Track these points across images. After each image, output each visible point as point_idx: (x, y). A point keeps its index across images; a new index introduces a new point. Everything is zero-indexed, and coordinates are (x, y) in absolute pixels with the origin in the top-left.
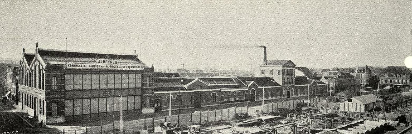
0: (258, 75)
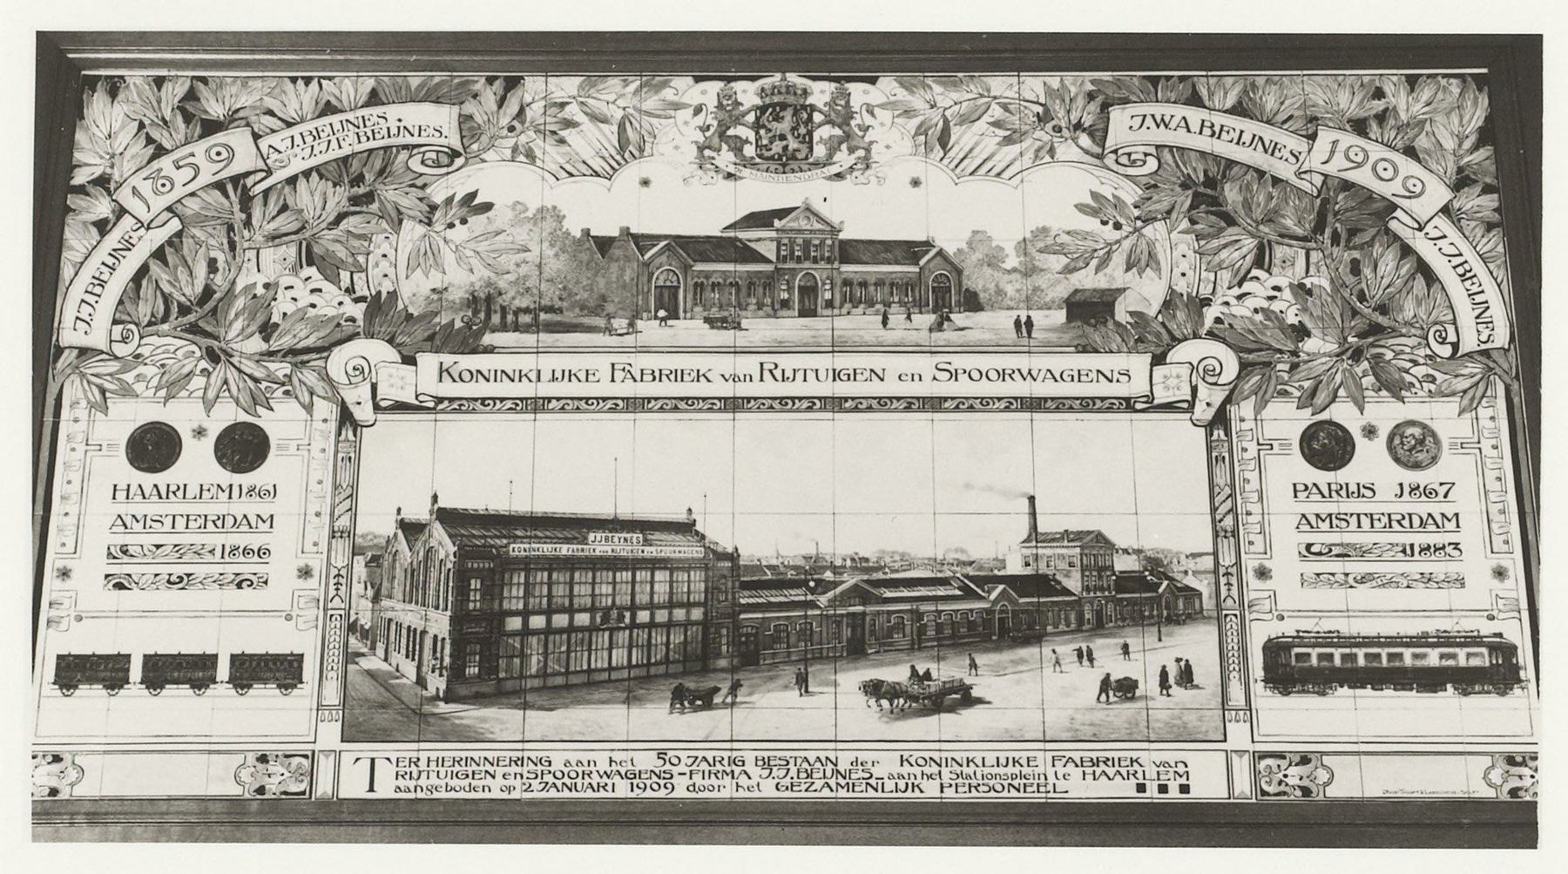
0: (1015, 567)
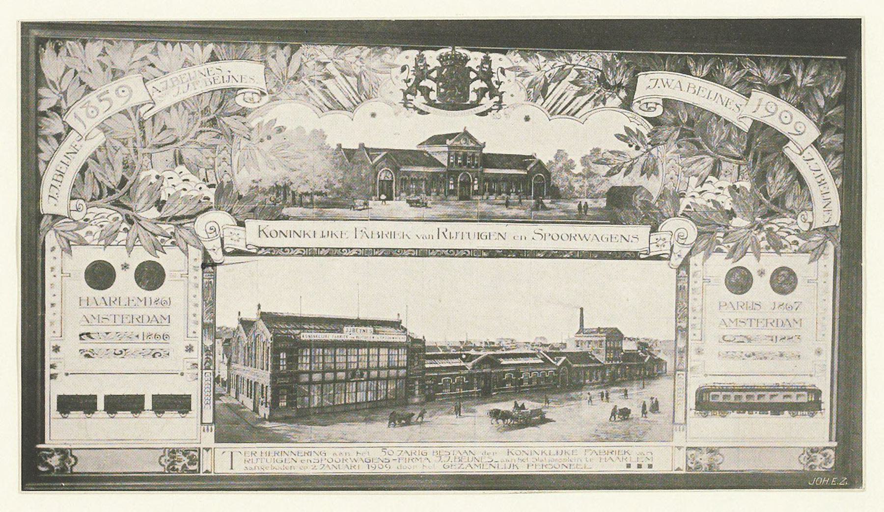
0: (571, 348)
